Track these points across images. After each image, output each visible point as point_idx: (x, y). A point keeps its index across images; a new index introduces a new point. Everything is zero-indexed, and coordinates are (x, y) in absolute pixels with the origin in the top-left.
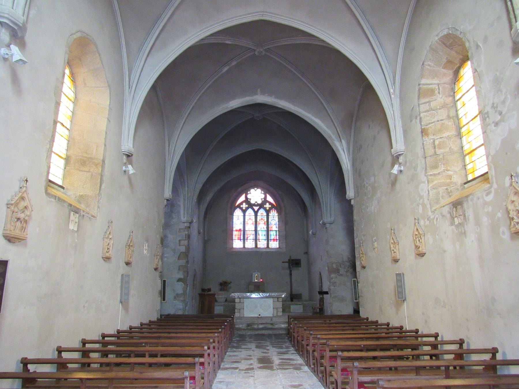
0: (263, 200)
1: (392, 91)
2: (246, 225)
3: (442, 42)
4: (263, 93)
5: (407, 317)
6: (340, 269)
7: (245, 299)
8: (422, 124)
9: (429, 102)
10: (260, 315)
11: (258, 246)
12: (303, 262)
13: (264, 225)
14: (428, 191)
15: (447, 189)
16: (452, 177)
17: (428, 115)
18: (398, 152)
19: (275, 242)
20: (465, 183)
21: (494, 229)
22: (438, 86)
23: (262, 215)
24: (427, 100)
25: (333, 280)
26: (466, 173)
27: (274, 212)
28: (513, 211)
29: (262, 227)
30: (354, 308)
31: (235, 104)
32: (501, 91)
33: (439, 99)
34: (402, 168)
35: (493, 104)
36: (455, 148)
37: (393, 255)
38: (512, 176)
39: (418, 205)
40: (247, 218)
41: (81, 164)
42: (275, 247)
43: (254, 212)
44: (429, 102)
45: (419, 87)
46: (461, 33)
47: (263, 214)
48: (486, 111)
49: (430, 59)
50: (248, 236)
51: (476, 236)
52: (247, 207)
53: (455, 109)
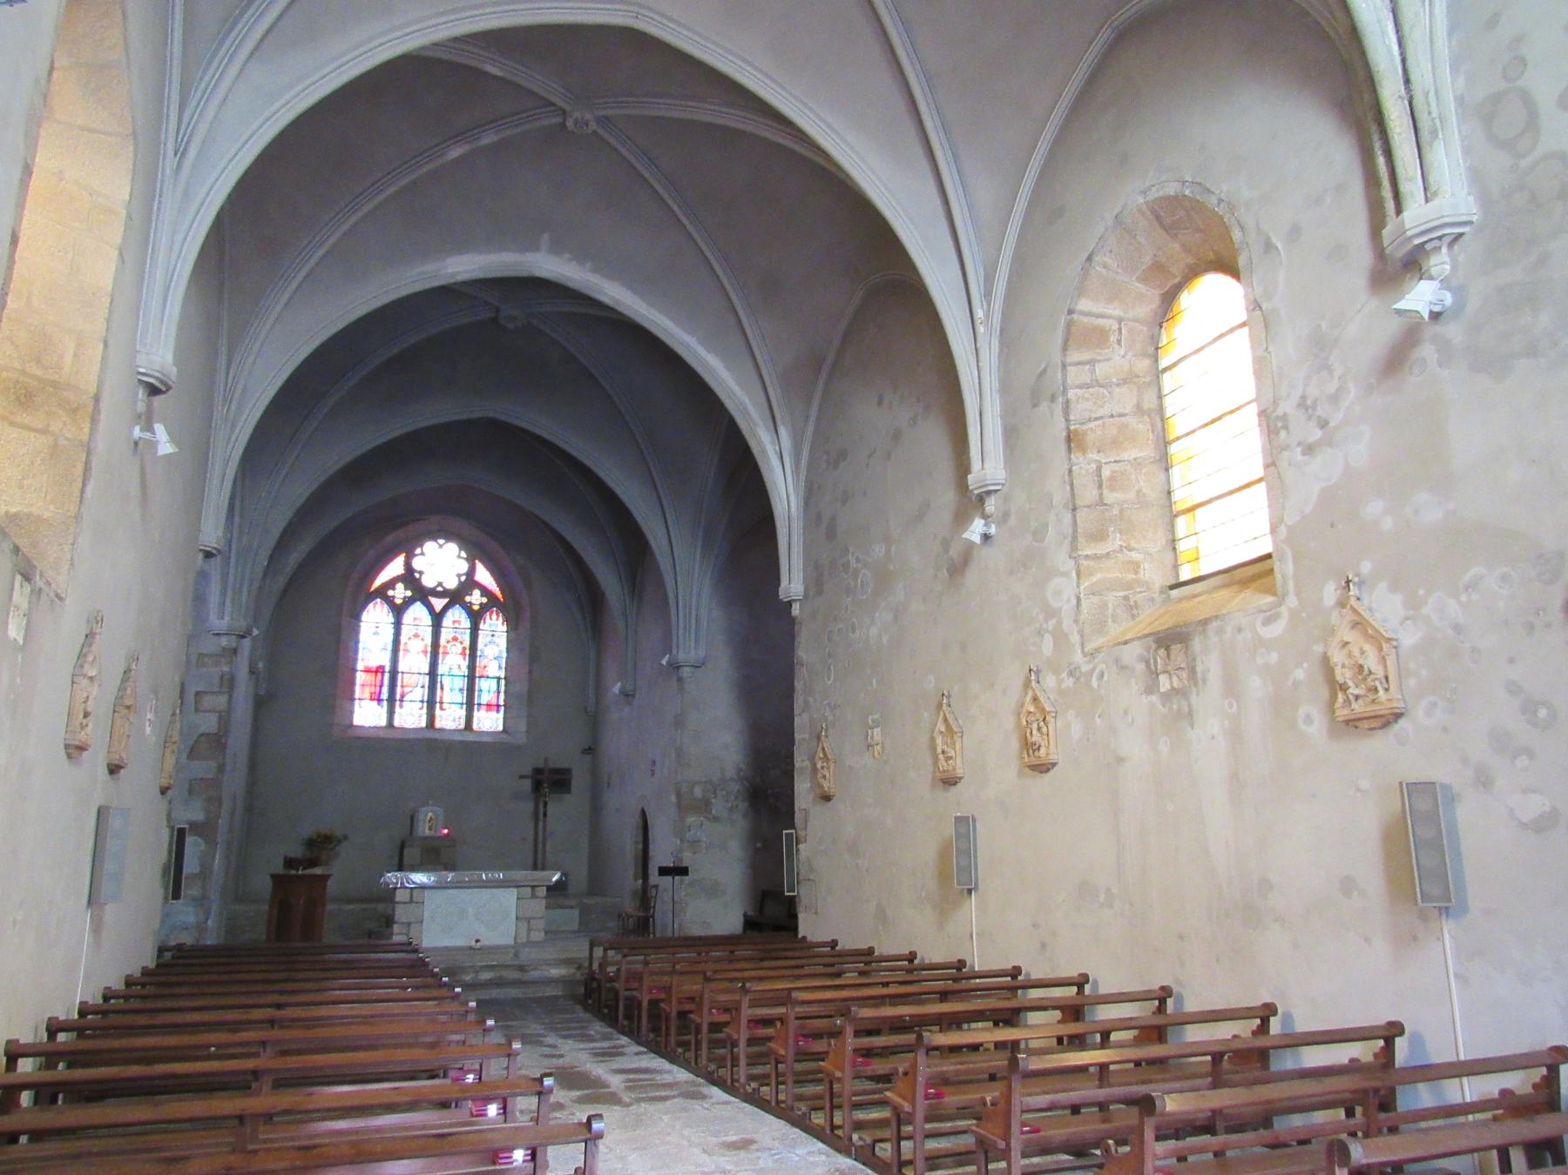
0: (463, 578)
1: (979, 313)
2: (401, 653)
3: (1152, 213)
4: (557, 248)
5: (978, 934)
6: (713, 801)
7: (426, 891)
8: (1072, 417)
9: (1092, 362)
10: (477, 941)
11: (438, 724)
12: (579, 781)
13: (461, 657)
14: (1078, 599)
15: (1126, 598)
16: (1139, 567)
17: (1086, 396)
18: (987, 485)
19: (493, 714)
20: (1172, 587)
21: (1281, 705)
22: (1120, 323)
23: (457, 625)
24: (1085, 356)
25: (692, 832)
26: (1176, 560)
27: (497, 619)
28: (1343, 666)
29: (453, 663)
30: (745, 915)
31: (464, 266)
32: (1331, 372)
33: (1118, 359)
34: (993, 530)
35: (1304, 398)
36: (1153, 493)
37: (943, 765)
38: (1348, 582)
39: (1039, 632)
40: (406, 631)
41: (18, 399)
42: (492, 730)
43: (430, 614)
44: (1092, 362)
45: (1069, 317)
46: (1220, 201)
47: (459, 622)
48: (1280, 412)
49: (1111, 252)
50: (406, 690)
51: (1226, 723)
52: (409, 598)
53: (1156, 389)
